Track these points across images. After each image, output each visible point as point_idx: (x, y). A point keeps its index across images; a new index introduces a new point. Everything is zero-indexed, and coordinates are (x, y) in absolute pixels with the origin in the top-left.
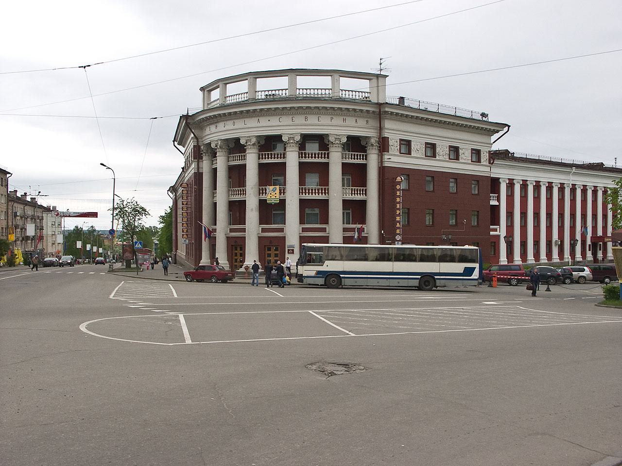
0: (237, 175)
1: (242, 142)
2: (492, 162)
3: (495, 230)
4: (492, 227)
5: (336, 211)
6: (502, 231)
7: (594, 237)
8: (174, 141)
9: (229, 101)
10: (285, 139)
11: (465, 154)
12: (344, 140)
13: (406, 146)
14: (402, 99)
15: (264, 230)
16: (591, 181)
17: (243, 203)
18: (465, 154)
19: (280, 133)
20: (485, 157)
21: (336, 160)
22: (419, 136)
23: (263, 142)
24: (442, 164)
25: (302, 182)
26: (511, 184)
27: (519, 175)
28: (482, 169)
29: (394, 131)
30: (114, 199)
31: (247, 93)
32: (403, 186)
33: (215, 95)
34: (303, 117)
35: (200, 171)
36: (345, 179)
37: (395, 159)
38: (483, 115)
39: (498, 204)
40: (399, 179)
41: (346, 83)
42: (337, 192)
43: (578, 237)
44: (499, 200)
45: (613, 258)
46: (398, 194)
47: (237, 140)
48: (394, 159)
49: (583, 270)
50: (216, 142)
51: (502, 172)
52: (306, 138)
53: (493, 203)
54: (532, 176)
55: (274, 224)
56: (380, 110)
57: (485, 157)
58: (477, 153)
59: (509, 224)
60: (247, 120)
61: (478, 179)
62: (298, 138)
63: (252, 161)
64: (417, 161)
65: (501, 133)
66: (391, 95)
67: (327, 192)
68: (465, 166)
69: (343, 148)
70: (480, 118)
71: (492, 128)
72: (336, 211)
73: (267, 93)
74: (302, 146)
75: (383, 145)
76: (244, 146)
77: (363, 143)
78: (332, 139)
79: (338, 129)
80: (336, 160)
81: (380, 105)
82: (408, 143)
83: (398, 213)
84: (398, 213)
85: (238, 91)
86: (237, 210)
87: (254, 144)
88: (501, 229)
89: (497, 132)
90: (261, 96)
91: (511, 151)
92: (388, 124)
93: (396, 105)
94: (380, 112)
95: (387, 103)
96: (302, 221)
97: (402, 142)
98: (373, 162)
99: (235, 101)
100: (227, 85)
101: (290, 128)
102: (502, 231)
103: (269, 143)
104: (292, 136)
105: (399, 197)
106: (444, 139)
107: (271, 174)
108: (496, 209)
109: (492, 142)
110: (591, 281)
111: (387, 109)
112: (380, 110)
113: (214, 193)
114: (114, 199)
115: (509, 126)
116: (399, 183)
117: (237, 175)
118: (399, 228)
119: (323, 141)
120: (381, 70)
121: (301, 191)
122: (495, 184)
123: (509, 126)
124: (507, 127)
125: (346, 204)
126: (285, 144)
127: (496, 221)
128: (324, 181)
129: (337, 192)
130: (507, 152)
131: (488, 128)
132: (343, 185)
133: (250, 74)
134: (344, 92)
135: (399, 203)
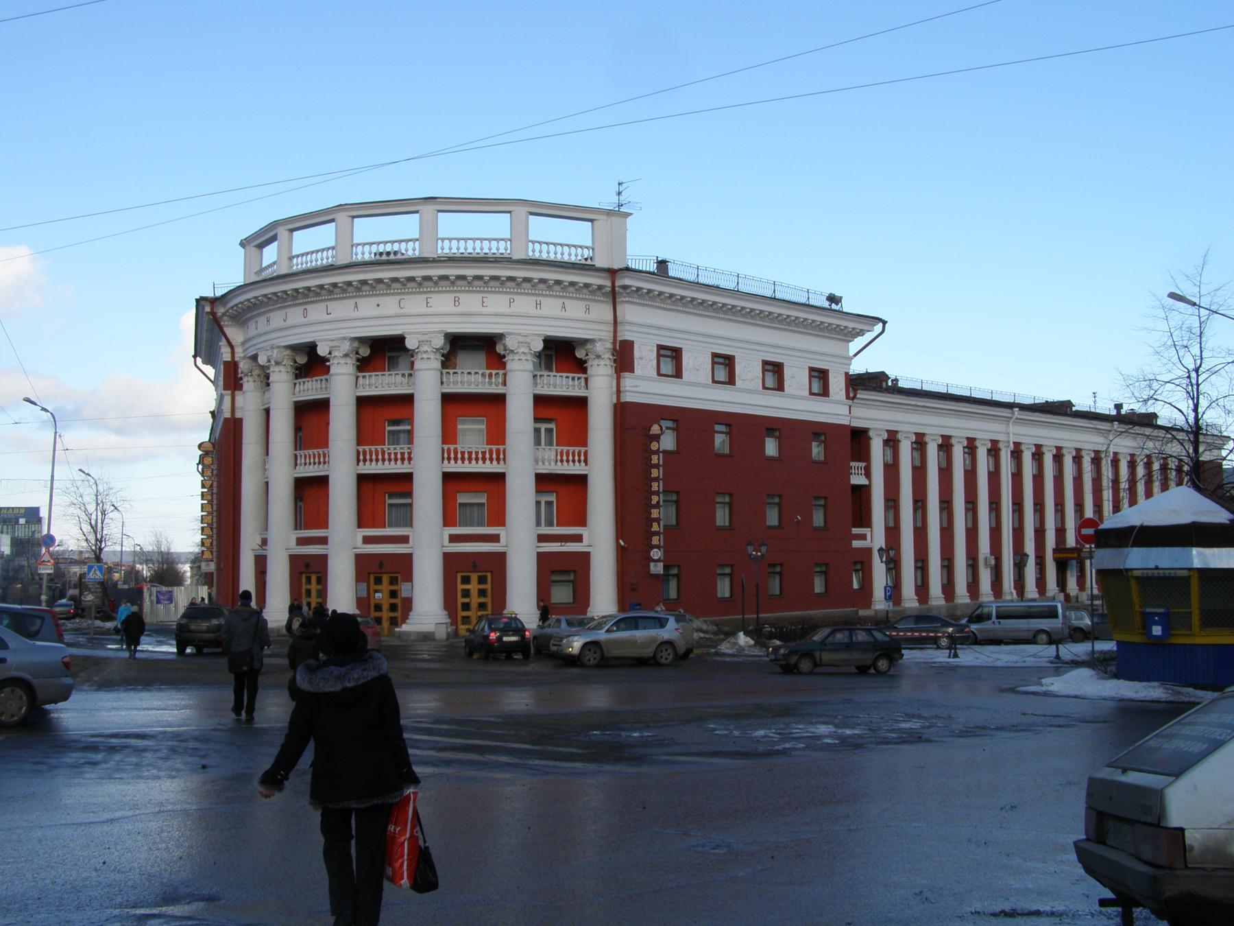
0: (311, 418)
1: (322, 351)
2: (851, 395)
3: (863, 537)
4: (855, 531)
5: (521, 497)
6: (876, 537)
7: (1060, 548)
8: (195, 357)
9: (298, 265)
10: (410, 343)
11: (797, 378)
12: (539, 346)
13: (672, 357)
14: (662, 264)
15: (301, 542)
16: (1052, 435)
17: (323, 481)
18: (797, 378)
19: (399, 332)
20: (837, 385)
21: (521, 385)
22: (701, 339)
23: (365, 352)
24: (747, 397)
25: (448, 435)
26: (892, 441)
27: (907, 421)
28: (835, 410)
29: (646, 326)
30: (52, 476)
31: (333, 248)
32: (668, 442)
33: (270, 254)
34: (451, 297)
35: (238, 415)
36: (543, 430)
37: (647, 386)
38: (833, 299)
39: (866, 482)
40: (655, 429)
41: (541, 228)
42: (524, 456)
43: (1030, 547)
44: (868, 474)
45: (853, 464)
46: (655, 459)
47: (311, 348)
48: (645, 387)
49: (661, 623)
50: (269, 353)
51: (873, 416)
52: (458, 345)
53: (857, 479)
54: (934, 424)
55: (390, 526)
56: (613, 284)
57: (837, 385)
58: (820, 376)
59: (891, 524)
60: (331, 305)
61: (819, 431)
62: (439, 341)
63: (342, 388)
64: (696, 390)
65: (869, 336)
66: (640, 252)
67: (501, 457)
68: (795, 403)
69: (538, 366)
70: (826, 304)
71: (851, 325)
72: (521, 497)
73: (381, 248)
74: (448, 361)
75: (623, 358)
76: (324, 360)
77: (580, 354)
78: (510, 342)
79: (526, 321)
80: (521, 385)
81: (612, 273)
82: (675, 354)
83: (654, 502)
84: (654, 502)
85: (313, 244)
86: (310, 494)
87: (346, 355)
88: (875, 537)
89: (861, 333)
90: (366, 254)
91: (892, 373)
92: (631, 313)
93: (652, 273)
94: (614, 283)
95: (628, 269)
96: (448, 520)
97: (662, 352)
98: (599, 388)
99: (319, 263)
100: (295, 233)
101: (424, 319)
102: (876, 537)
103: (384, 351)
104: (425, 338)
105: (657, 466)
106: (751, 346)
107: (383, 416)
108: (861, 494)
109: (851, 354)
110: (149, 906)
111: (627, 282)
112: (613, 284)
113: (265, 463)
114: (52, 476)
115: (884, 323)
116: (657, 438)
117: (311, 418)
118: (657, 533)
119: (487, 347)
120: (620, 205)
121: (446, 456)
122: (858, 439)
123: (884, 323)
124: (881, 325)
125: (544, 481)
126: (411, 354)
127: (863, 518)
128: (497, 434)
129: (524, 456)
130: (881, 377)
131: (835, 321)
132: (537, 442)
133: (340, 208)
134: (537, 245)
135: (657, 479)
